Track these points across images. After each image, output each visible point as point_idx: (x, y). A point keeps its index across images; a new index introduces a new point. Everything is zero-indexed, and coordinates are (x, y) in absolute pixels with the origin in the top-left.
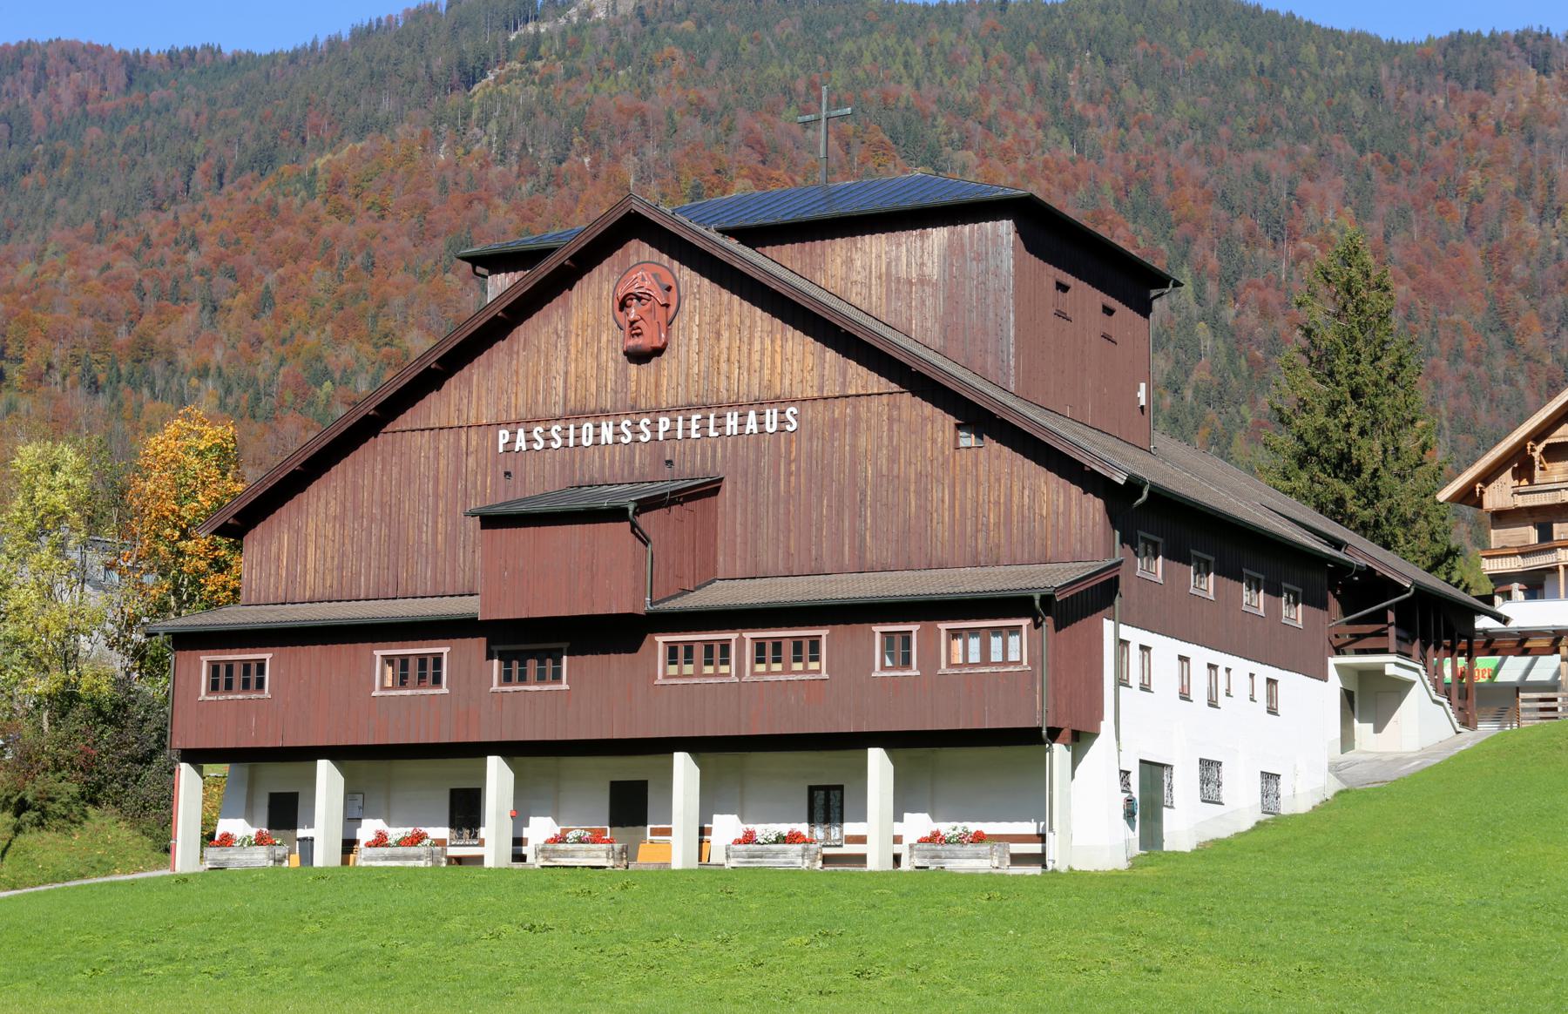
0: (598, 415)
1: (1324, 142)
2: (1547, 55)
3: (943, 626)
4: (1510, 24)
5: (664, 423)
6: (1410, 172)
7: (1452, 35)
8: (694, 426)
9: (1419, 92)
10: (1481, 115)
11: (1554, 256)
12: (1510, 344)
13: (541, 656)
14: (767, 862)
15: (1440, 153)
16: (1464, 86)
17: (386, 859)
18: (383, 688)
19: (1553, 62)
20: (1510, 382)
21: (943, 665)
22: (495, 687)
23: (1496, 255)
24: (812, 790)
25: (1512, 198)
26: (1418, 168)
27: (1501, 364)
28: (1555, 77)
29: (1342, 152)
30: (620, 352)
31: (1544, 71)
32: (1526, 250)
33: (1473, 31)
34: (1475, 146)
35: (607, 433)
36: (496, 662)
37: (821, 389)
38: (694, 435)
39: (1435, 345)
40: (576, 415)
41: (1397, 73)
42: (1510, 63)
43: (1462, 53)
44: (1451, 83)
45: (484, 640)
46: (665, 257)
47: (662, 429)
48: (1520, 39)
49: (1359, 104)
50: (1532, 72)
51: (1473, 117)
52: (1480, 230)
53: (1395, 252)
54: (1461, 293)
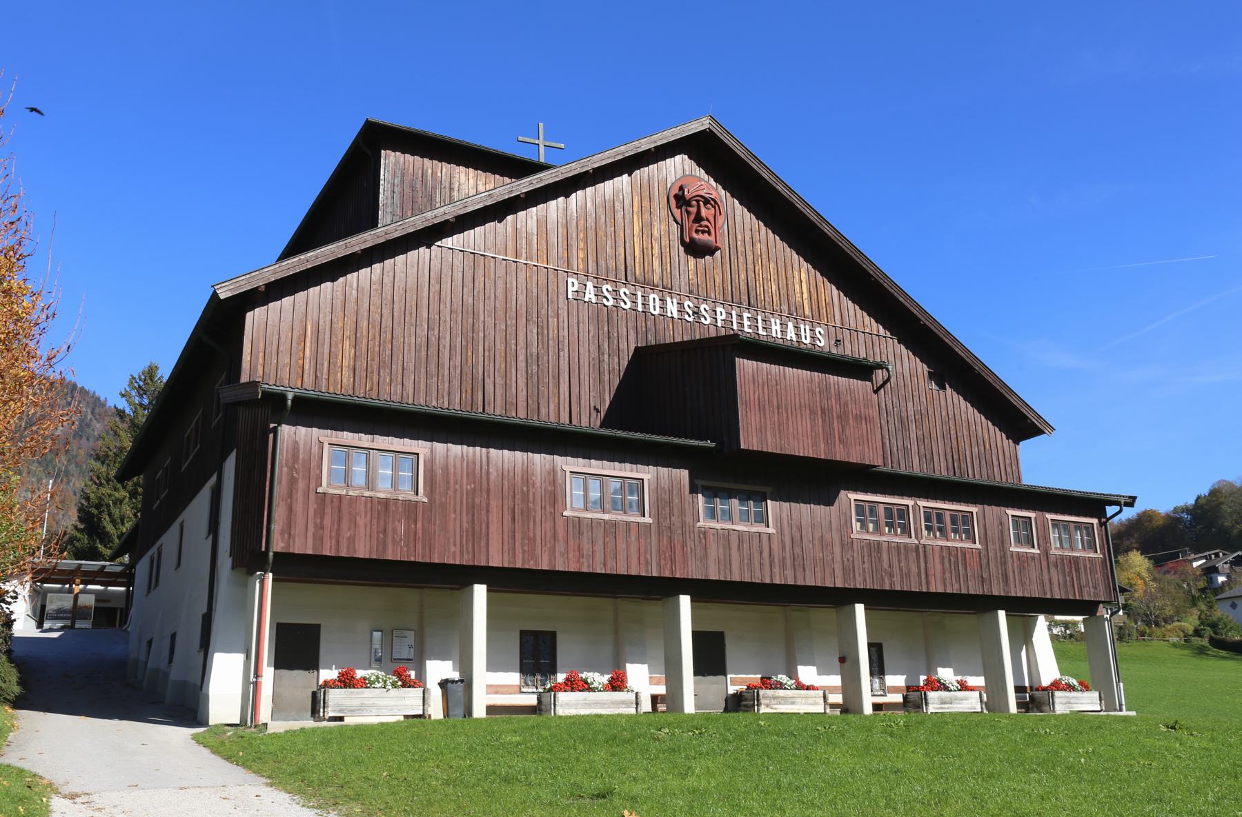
3: (1050, 516)
8: (746, 323)
17: (589, 705)
22: (701, 524)
47: (719, 318)
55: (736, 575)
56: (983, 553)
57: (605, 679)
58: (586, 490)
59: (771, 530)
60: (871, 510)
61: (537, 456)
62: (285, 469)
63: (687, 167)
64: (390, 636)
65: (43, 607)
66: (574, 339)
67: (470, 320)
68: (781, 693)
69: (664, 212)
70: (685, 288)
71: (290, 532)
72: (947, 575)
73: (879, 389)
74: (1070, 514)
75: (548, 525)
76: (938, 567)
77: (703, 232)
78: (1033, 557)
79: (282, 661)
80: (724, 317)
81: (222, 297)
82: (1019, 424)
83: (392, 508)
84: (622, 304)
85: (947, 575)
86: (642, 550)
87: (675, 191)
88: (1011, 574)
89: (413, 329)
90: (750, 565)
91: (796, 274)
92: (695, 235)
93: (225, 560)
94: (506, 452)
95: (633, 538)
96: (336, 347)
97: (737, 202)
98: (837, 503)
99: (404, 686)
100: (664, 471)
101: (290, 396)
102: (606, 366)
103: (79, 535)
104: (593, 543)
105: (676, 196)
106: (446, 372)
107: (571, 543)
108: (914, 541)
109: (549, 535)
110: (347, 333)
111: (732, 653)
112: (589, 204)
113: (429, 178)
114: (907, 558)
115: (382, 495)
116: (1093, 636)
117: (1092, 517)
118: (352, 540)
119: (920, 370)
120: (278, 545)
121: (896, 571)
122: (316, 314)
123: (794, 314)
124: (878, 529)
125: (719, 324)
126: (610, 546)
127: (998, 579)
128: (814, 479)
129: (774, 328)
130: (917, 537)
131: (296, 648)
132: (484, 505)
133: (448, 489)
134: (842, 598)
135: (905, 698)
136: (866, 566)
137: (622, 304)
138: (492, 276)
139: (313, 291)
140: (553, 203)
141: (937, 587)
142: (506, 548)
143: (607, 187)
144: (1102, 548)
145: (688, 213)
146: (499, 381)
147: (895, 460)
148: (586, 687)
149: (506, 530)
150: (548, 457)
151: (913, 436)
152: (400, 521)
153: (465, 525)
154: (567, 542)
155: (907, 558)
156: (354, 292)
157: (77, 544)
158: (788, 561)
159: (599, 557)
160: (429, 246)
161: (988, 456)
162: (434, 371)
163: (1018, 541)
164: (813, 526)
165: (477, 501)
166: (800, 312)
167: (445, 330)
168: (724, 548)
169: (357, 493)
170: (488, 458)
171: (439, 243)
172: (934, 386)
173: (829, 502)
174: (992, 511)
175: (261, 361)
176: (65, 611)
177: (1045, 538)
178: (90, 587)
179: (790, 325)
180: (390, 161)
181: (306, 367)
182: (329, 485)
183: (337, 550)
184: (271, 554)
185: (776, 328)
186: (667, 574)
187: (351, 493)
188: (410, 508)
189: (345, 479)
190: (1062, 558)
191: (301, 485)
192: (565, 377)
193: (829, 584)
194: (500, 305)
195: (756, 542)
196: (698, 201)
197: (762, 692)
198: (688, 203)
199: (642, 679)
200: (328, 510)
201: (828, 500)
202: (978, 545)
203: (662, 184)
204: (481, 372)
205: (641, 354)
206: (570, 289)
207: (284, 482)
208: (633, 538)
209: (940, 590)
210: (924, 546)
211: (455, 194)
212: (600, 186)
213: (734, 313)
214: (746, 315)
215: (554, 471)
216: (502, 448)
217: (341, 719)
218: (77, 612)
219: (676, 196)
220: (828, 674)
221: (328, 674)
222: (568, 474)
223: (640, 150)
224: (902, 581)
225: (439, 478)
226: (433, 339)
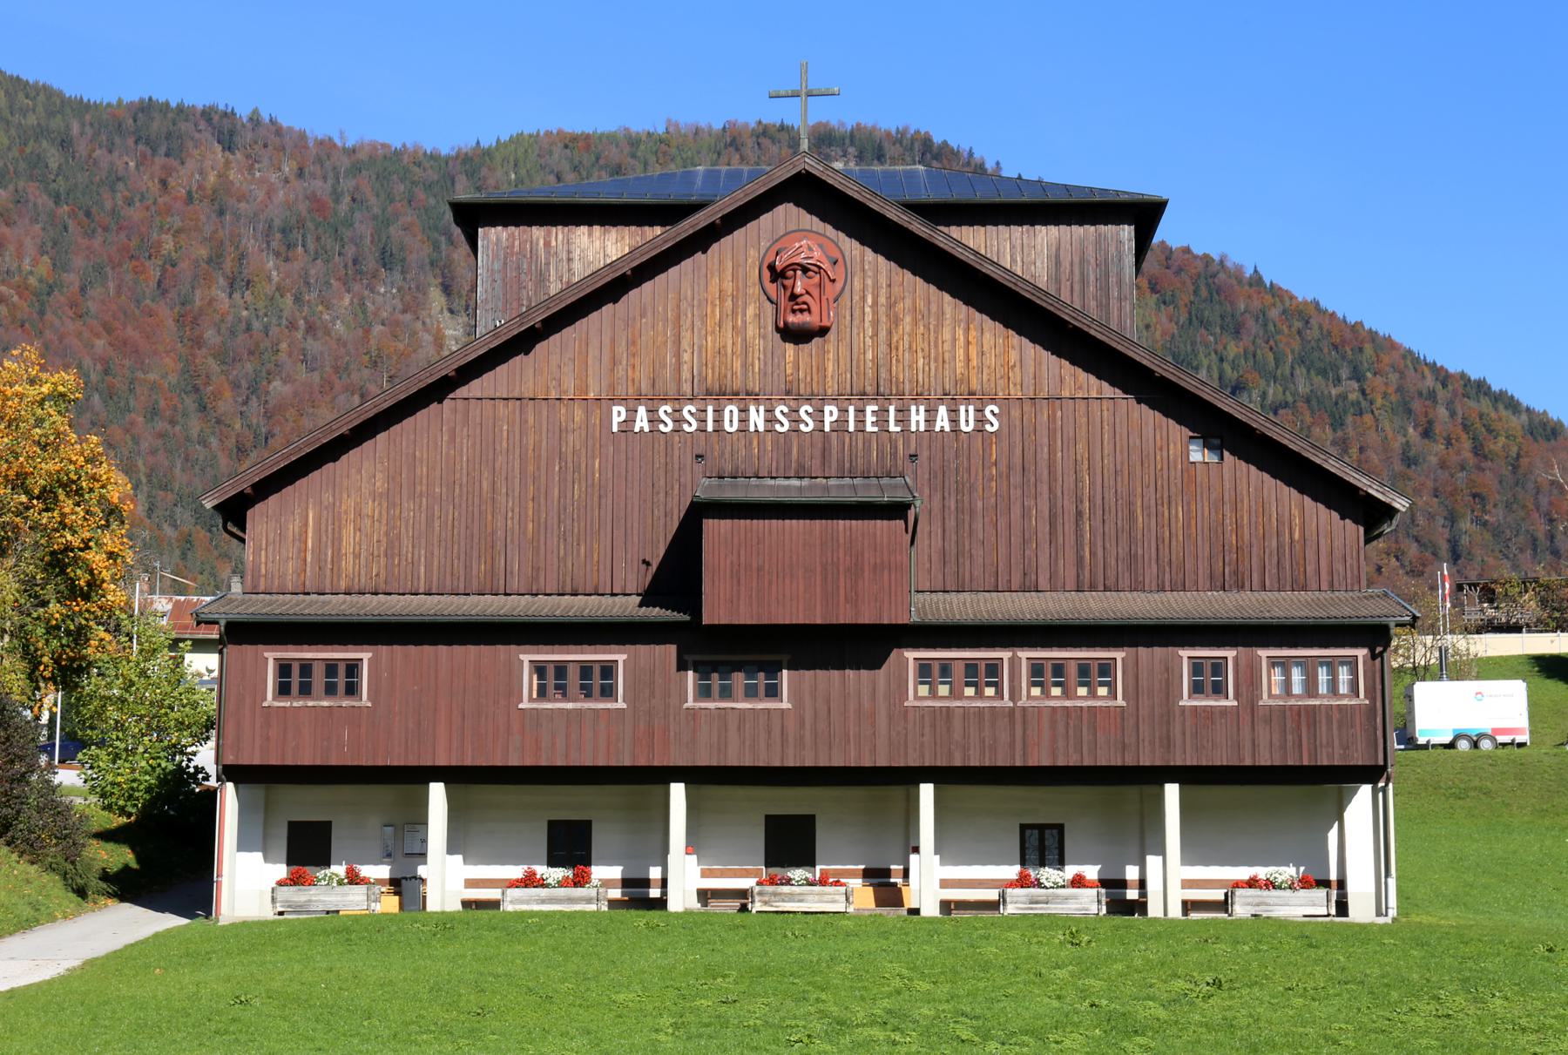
0: (744, 397)
1: (20, 188)
2: (232, 133)
3: (1264, 653)
4: (197, 99)
5: (831, 413)
6: (106, 229)
7: (142, 101)
8: (870, 419)
9: (110, 152)
10: (172, 182)
11: (243, 326)
12: (203, 408)
13: (751, 668)
14: (1053, 909)
15: (135, 214)
16: (154, 150)
17: (543, 902)
18: (531, 700)
19: (237, 139)
20: (204, 443)
21: (1265, 696)
22: (690, 703)
23: (189, 320)
24: (1024, 828)
25: (204, 265)
26: (114, 227)
27: (195, 425)
28: (239, 155)
29: (40, 201)
30: (770, 327)
31: (229, 147)
32: (217, 317)
33: (162, 100)
34: (168, 210)
35: (757, 419)
36: (690, 673)
37: (612, 387)
38: (869, 428)
39: (132, 403)
40: (720, 394)
41: (88, 129)
42: (197, 135)
43: (153, 119)
44: (141, 147)
45: (673, 649)
46: (829, 227)
47: (828, 420)
48: (207, 114)
49: (54, 158)
50: (219, 148)
51: (164, 183)
52: (173, 294)
53: (92, 306)
54: (155, 353)
68: (786, 889)
69: (757, 288)
76: (1046, 734)
77: (801, 311)
99: (351, 883)
108: (1007, 702)
124: (955, 694)
125: (827, 429)
127: (1152, 743)
129: (914, 418)
130: (1012, 698)
136: (925, 739)
145: (785, 287)
153: (411, 725)
160: (704, 252)
179: (942, 410)
195: (776, 722)
220: (476, 864)
224: (983, 753)
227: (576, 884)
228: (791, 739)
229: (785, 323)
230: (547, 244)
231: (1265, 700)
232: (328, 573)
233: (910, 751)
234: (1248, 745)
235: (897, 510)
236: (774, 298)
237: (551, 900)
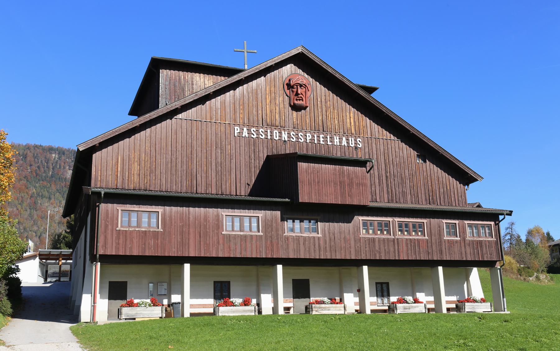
3: (466, 222)
8: (321, 139)
17: (234, 312)
38: (322, 142)
47: (308, 138)
55: (302, 255)
56: (429, 241)
57: (240, 301)
58: (233, 222)
59: (320, 235)
60: (371, 224)
61: (211, 209)
62: (103, 221)
63: (293, 70)
64: (156, 285)
65: (47, 271)
66: (238, 154)
67: (190, 150)
68: (323, 305)
70: (291, 126)
71: (106, 246)
72: (409, 252)
73: (369, 170)
74: (479, 220)
75: (215, 238)
76: (405, 248)
77: (300, 100)
78: (457, 241)
79: (111, 297)
80: (310, 138)
81: (81, 150)
82: (465, 177)
83: (148, 234)
84: (261, 136)
85: (409, 252)
86: (258, 247)
87: (287, 82)
88: (444, 250)
89: (165, 156)
90: (309, 251)
91: (348, 114)
92: (296, 102)
93: (88, 257)
94: (197, 209)
95: (254, 242)
96: (131, 165)
97: (318, 83)
98: (352, 222)
99: (154, 306)
100: (269, 212)
101: (103, 193)
102: (253, 165)
103: (67, 235)
104: (236, 245)
105: (287, 84)
106: (180, 173)
107: (226, 245)
108: (392, 237)
109: (215, 242)
110: (136, 160)
111: (313, 289)
112: (245, 92)
113: (182, 80)
114: (388, 245)
115: (143, 230)
116: (493, 276)
117: (490, 221)
118: (131, 248)
119: (412, 154)
120: (101, 251)
121: (382, 250)
122: (122, 153)
123: (347, 134)
124: (374, 233)
125: (308, 141)
126: (243, 246)
127: (436, 252)
128: (342, 212)
129: (335, 140)
130: (394, 235)
131: (117, 292)
132: (187, 231)
133: (172, 225)
134: (358, 263)
135: (457, 306)
136: (367, 249)
137: (261, 136)
138: (200, 129)
139: (121, 143)
140: (228, 94)
141: (404, 257)
142: (197, 249)
143: (254, 83)
144: (496, 236)
145: (293, 91)
146: (204, 175)
147: (398, 198)
148: (232, 304)
149: (197, 241)
150: (215, 209)
151: (408, 186)
152: (151, 240)
153: (179, 239)
154: (224, 245)
155: (388, 245)
156: (139, 142)
157: (66, 239)
158: (328, 249)
159: (238, 250)
160: (171, 119)
161: (449, 193)
162: (174, 173)
163: (449, 234)
164: (340, 233)
165: (184, 230)
166: (349, 132)
167: (179, 154)
168: (297, 244)
169: (133, 229)
170: (189, 211)
171: (175, 117)
172: (421, 161)
173: (349, 221)
174: (434, 221)
175: (99, 174)
176: (56, 273)
177: (463, 232)
178: (68, 261)
179: (344, 139)
180: (164, 75)
181: (119, 175)
182: (121, 226)
183: (125, 252)
184: (98, 255)
185: (336, 141)
186: (270, 256)
187: (130, 229)
188: (156, 234)
189: (126, 225)
190: (473, 241)
191: (110, 227)
192: (233, 171)
193: (348, 258)
194: (204, 142)
195: (312, 241)
196: (297, 86)
197: (397, 305)
198: (293, 87)
199: (351, 301)
200: (121, 237)
201: (349, 220)
202: (426, 237)
203: (280, 79)
204: (195, 171)
205: (269, 159)
206: (236, 132)
207: (103, 226)
208: (254, 242)
209: (405, 259)
210: (398, 239)
211: (195, 86)
212: (250, 83)
213: (315, 136)
214: (321, 136)
215: (218, 215)
216: (195, 207)
217: (134, 319)
218: (61, 274)
219: (287, 84)
221: (393, 299)
222: (224, 216)
223: (267, 66)
224: (385, 255)
225: (168, 222)
226: (174, 159)
227: (245, 305)
228: (322, 249)
229: (294, 104)
230: (184, 78)
231: (468, 238)
232: (127, 181)
233: (362, 253)
234: (464, 253)
235: (361, 163)
236: (289, 95)
237: (237, 311)
